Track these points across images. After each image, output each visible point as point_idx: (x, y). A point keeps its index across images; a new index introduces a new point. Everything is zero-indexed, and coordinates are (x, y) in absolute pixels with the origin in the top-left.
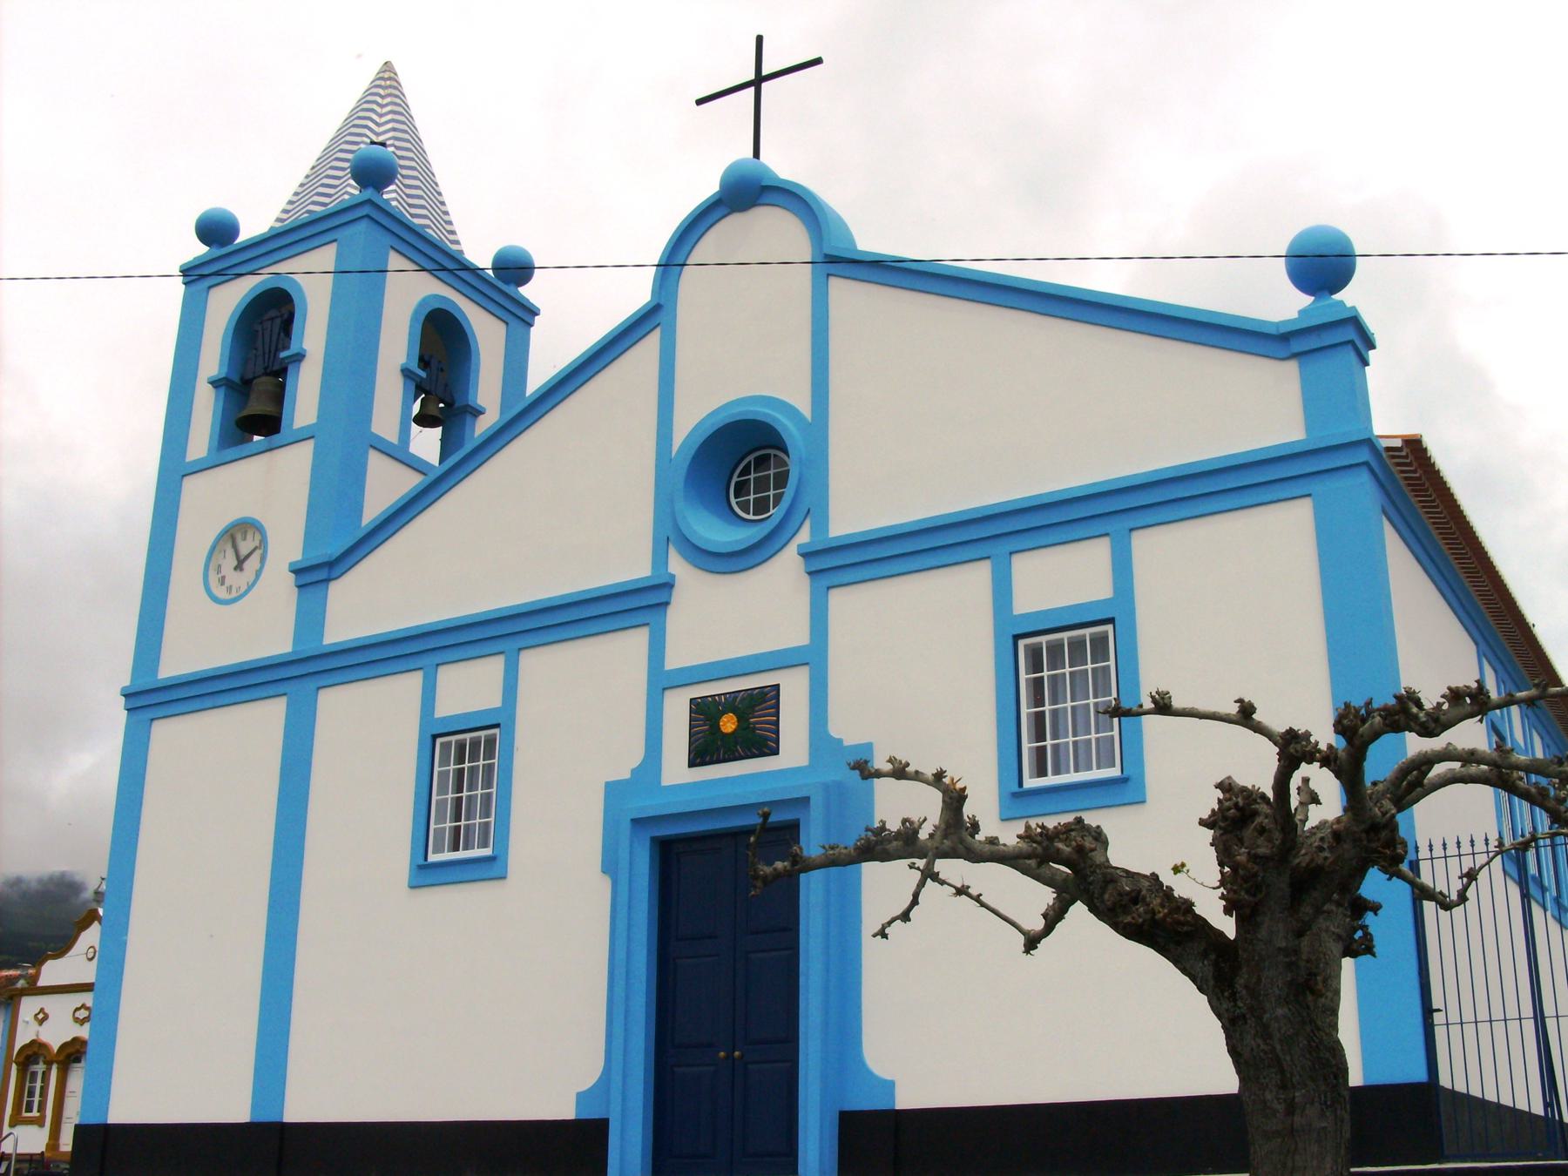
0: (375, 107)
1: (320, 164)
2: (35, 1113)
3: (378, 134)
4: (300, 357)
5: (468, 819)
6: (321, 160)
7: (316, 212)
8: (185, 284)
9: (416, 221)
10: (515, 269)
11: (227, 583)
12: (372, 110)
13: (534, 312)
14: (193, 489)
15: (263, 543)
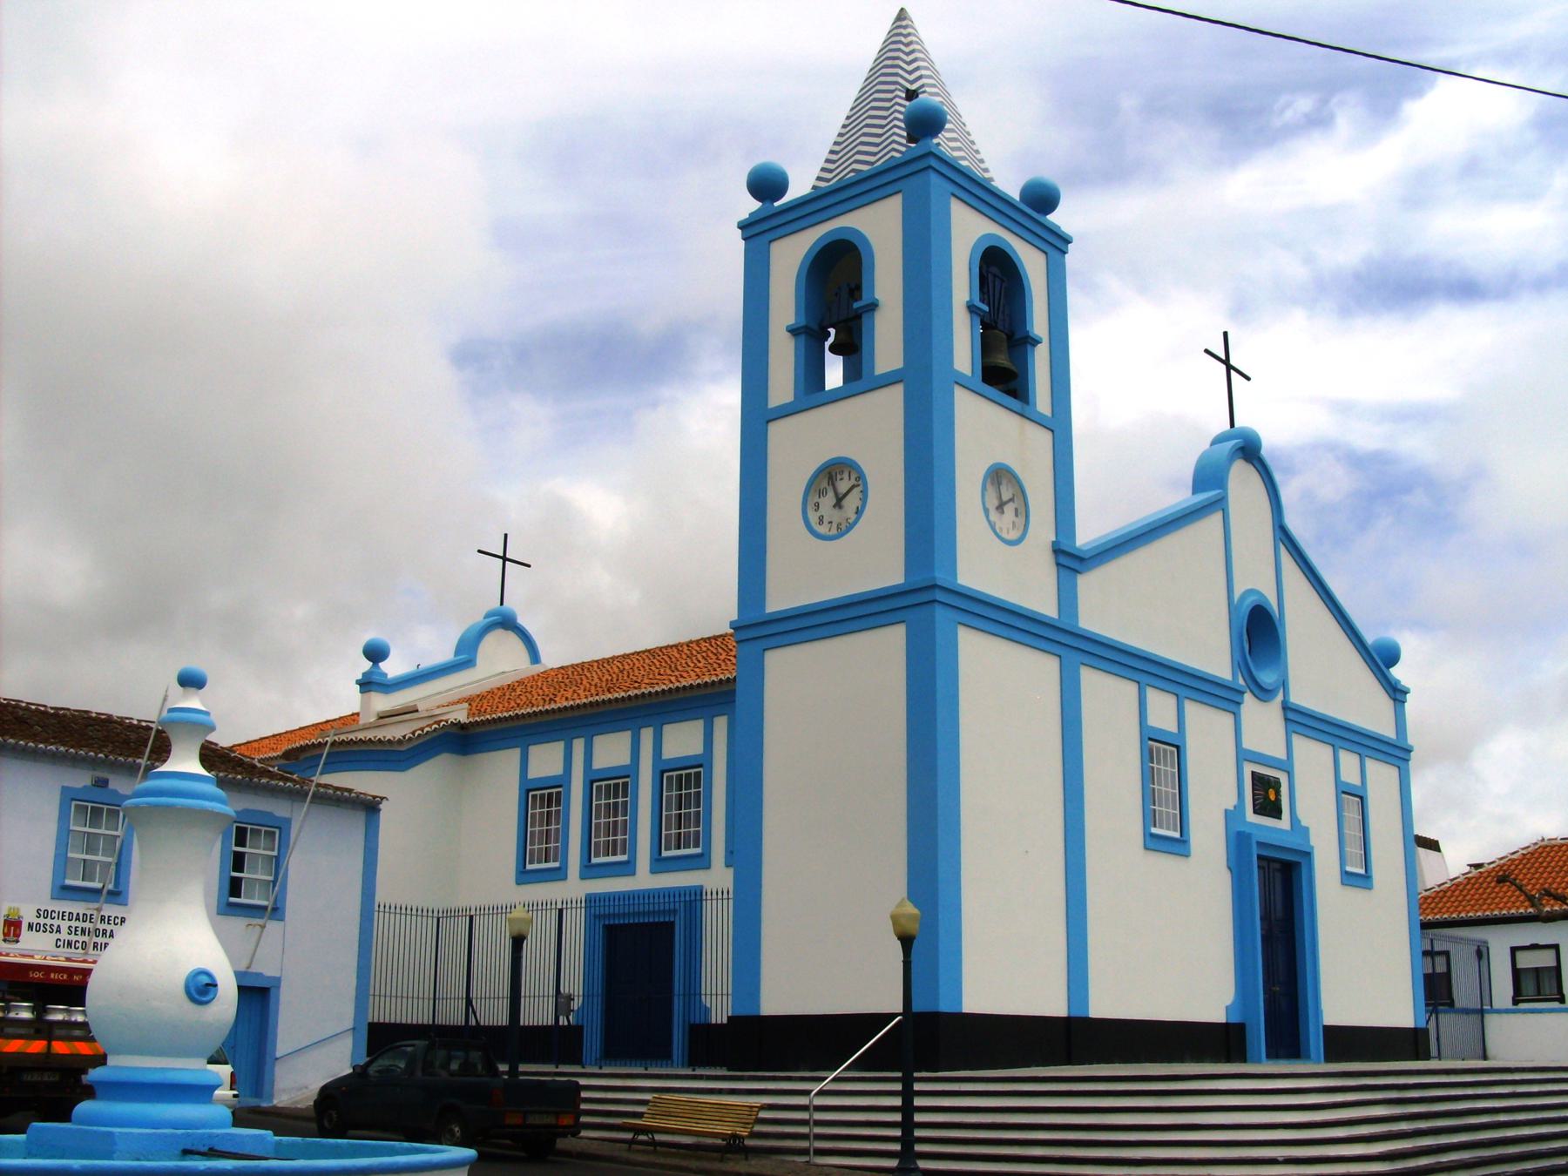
1: (854, 114)
3: (912, 82)
4: (873, 306)
5: (680, 833)
6: (859, 101)
7: (861, 171)
8: (744, 239)
9: (956, 154)
10: (1042, 199)
12: (899, 50)
13: (1067, 240)
14: (778, 433)
15: (861, 477)
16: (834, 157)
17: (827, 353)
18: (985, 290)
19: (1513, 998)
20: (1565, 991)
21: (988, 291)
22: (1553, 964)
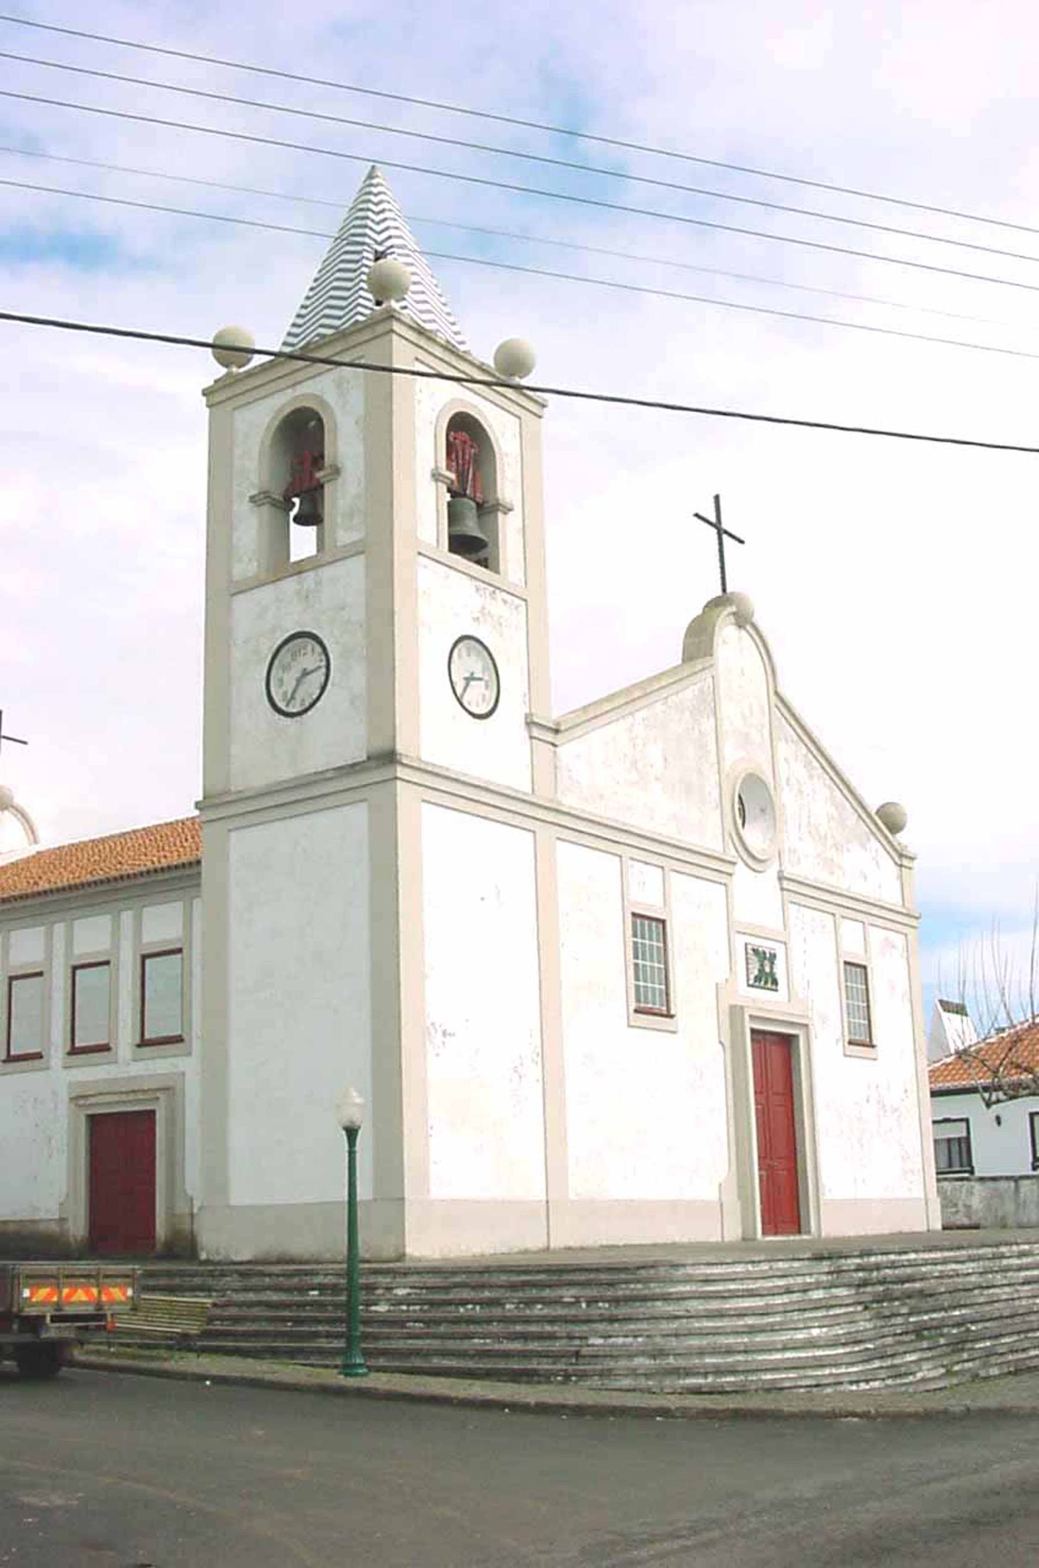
0: (370, 214)
2: (762, 983)
3: (380, 244)
8: (208, 406)
11: (93, 885)
16: (300, 321)
17: (293, 525)
18: (453, 456)
19: (1033, 1164)
20: (974, 1163)
21: (457, 457)
22: (964, 1134)
